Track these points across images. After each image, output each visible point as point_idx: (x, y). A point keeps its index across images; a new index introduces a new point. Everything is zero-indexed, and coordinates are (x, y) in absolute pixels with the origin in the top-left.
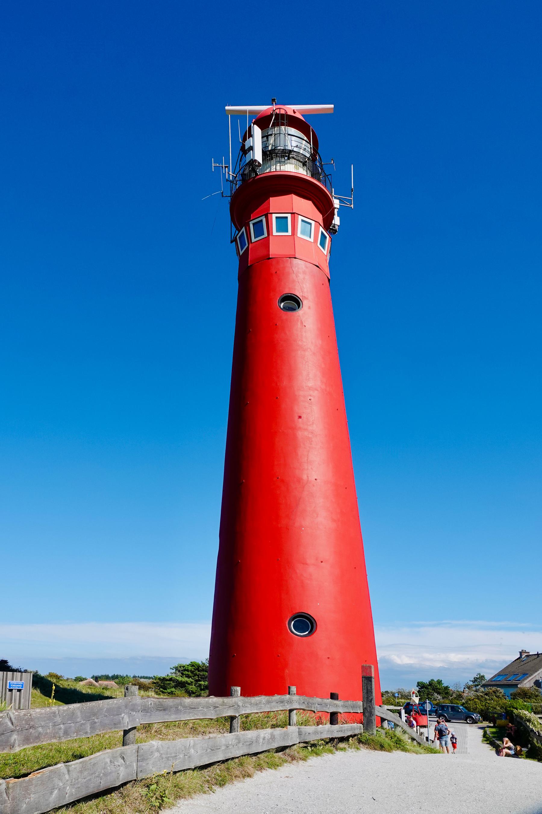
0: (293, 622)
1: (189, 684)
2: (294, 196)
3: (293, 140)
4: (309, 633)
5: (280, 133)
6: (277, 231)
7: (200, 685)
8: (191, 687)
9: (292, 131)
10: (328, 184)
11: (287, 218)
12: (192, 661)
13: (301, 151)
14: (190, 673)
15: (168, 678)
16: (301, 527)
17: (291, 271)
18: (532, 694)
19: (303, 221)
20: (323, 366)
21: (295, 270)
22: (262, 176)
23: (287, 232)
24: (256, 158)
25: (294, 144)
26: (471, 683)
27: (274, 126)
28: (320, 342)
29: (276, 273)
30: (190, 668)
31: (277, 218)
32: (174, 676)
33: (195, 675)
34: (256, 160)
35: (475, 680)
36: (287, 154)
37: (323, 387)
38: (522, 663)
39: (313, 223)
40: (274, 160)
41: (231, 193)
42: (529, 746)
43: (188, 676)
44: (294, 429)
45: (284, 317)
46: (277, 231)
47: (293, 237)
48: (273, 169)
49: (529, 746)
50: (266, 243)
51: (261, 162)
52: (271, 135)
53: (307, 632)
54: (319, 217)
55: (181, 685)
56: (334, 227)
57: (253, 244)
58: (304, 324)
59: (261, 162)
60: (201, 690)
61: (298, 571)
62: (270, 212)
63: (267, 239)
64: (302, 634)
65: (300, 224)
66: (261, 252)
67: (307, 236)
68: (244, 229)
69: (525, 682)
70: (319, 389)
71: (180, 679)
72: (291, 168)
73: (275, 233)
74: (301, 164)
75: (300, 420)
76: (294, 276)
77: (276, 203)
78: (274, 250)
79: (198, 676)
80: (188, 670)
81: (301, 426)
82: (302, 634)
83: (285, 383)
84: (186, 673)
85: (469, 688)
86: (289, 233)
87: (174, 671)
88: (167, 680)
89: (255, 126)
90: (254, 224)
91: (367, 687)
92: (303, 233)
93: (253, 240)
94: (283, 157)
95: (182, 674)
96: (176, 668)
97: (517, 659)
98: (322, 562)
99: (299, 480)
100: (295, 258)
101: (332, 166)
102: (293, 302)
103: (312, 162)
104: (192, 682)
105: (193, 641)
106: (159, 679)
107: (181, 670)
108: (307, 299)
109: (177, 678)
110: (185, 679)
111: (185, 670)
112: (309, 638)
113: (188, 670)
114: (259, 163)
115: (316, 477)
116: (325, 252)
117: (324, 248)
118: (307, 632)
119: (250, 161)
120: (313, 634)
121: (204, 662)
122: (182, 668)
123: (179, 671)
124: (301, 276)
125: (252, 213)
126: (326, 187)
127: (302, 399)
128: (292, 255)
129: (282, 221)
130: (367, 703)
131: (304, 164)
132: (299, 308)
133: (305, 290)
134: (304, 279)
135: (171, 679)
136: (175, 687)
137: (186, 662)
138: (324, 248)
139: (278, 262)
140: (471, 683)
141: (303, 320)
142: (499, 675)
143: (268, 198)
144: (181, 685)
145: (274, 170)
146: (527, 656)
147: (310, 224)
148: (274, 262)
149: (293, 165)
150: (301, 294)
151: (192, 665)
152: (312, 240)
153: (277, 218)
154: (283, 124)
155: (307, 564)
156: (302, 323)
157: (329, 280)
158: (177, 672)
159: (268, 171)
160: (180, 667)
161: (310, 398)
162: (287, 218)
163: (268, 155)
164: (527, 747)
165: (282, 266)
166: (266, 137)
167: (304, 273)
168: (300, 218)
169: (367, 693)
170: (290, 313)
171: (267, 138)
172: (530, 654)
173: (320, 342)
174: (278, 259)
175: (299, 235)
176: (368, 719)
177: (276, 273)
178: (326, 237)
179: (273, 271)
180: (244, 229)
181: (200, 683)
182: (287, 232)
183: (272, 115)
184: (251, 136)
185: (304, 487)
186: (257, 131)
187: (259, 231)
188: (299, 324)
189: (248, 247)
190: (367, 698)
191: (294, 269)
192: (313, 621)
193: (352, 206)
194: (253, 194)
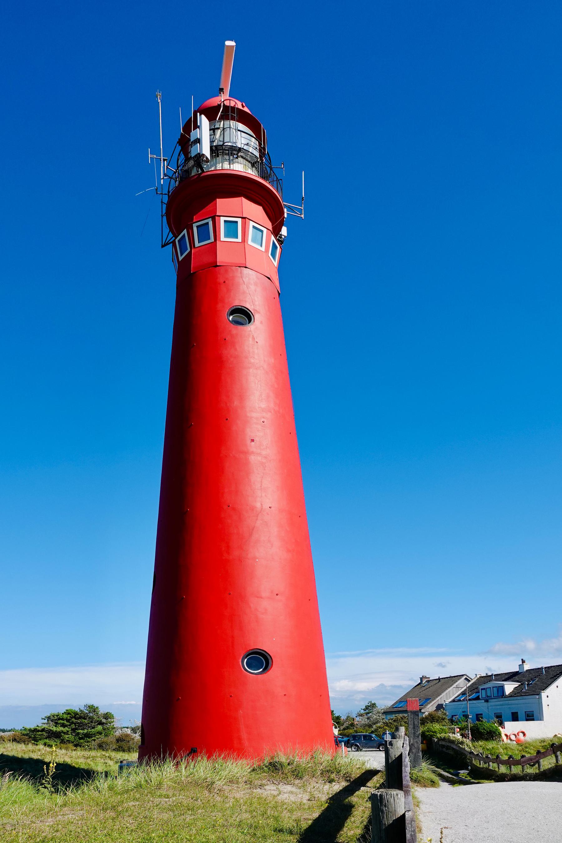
0: (246, 660)
1: (64, 733)
2: (244, 199)
3: (240, 136)
4: (264, 670)
5: (230, 128)
6: (226, 236)
7: (78, 734)
8: (67, 736)
9: (241, 126)
10: (279, 188)
11: (236, 222)
12: (68, 708)
13: (251, 150)
14: (65, 722)
15: (40, 729)
16: (255, 558)
17: (241, 281)
18: (439, 717)
19: (254, 227)
20: (276, 386)
21: (246, 280)
22: (209, 173)
23: (237, 238)
24: (204, 153)
25: (244, 141)
26: (362, 712)
27: (222, 118)
28: (272, 360)
29: (224, 282)
30: (65, 716)
31: (225, 221)
32: (46, 726)
33: (72, 723)
34: (203, 155)
35: (367, 708)
36: (234, 152)
37: (277, 408)
38: (424, 688)
39: (265, 230)
40: (220, 157)
41: (169, 192)
42: (470, 768)
43: (63, 726)
44: (246, 453)
45: (234, 332)
46: (226, 236)
47: (243, 244)
48: (219, 167)
49: (470, 768)
50: (212, 248)
51: (209, 157)
52: (218, 128)
53: (261, 670)
54: (270, 225)
55: (56, 735)
56: (281, 238)
57: (197, 250)
58: (256, 340)
59: (209, 157)
60: (80, 739)
61: (252, 605)
62: (217, 214)
63: (213, 246)
64: (256, 672)
65: (251, 230)
66: (206, 259)
67: (258, 244)
68: (185, 231)
69: (428, 707)
70: (272, 412)
71: (54, 729)
72: (240, 167)
73: (223, 238)
74: (250, 165)
75: (253, 443)
76: (243, 287)
77: (223, 205)
78: (222, 257)
79: (75, 724)
80: (63, 719)
81: (254, 450)
82: (256, 672)
83: (236, 403)
84: (62, 722)
85: (361, 715)
86: (239, 240)
87: (46, 721)
88: (39, 731)
89: (203, 116)
90: (197, 227)
91: (414, 722)
92: (253, 241)
93: (197, 244)
94: (232, 154)
95: (56, 723)
96: (49, 718)
97: (418, 685)
98: (277, 595)
99: (253, 508)
100: (246, 267)
101: (282, 172)
102: (244, 315)
103: (262, 162)
104: (68, 731)
105: (119, 686)
106: (30, 730)
107: (55, 719)
108: (259, 312)
109: (51, 728)
110: (60, 729)
111: (59, 719)
112: (265, 676)
113: (63, 719)
114: (207, 158)
115: (270, 506)
116: (276, 264)
117: (274, 258)
118: (261, 670)
119: (196, 156)
120: (268, 671)
121: (82, 709)
122: (56, 718)
123: (52, 721)
124: (252, 287)
125: (195, 215)
126: (277, 191)
127: (255, 421)
128: (242, 264)
129: (231, 226)
130: (413, 739)
131: (253, 165)
132: (249, 323)
133: (257, 303)
134: (255, 291)
135: (43, 730)
136: (48, 737)
137: (61, 710)
138: (274, 258)
139: (226, 271)
140: (362, 712)
141: (255, 336)
142: (400, 701)
143: (215, 199)
144: (56, 735)
145: (221, 168)
146: (428, 681)
147: (262, 231)
148: (222, 270)
149: (242, 165)
150: (253, 307)
151: (68, 713)
152: (263, 249)
153: (225, 221)
154: (233, 119)
155: (261, 598)
156: (253, 338)
157: (279, 294)
158: (50, 722)
159: (213, 169)
160: (53, 716)
161: (263, 420)
162: (236, 222)
163: (216, 150)
164: (467, 769)
165: (231, 275)
166: (213, 130)
167: (256, 284)
168: (252, 224)
169: (414, 728)
170: (240, 327)
171: (214, 132)
172: (431, 679)
173: (273, 361)
174: (226, 267)
175: (250, 242)
176: (415, 755)
177: (224, 282)
178: (276, 248)
179: (221, 280)
180: (185, 231)
181: (79, 731)
182: (237, 238)
183: (219, 106)
184: (196, 127)
185: (257, 516)
186: (204, 122)
187: (204, 236)
188: (251, 339)
189: (190, 253)
190: (414, 733)
191: (244, 280)
192: (269, 657)
193: (303, 216)
194: (194, 194)
